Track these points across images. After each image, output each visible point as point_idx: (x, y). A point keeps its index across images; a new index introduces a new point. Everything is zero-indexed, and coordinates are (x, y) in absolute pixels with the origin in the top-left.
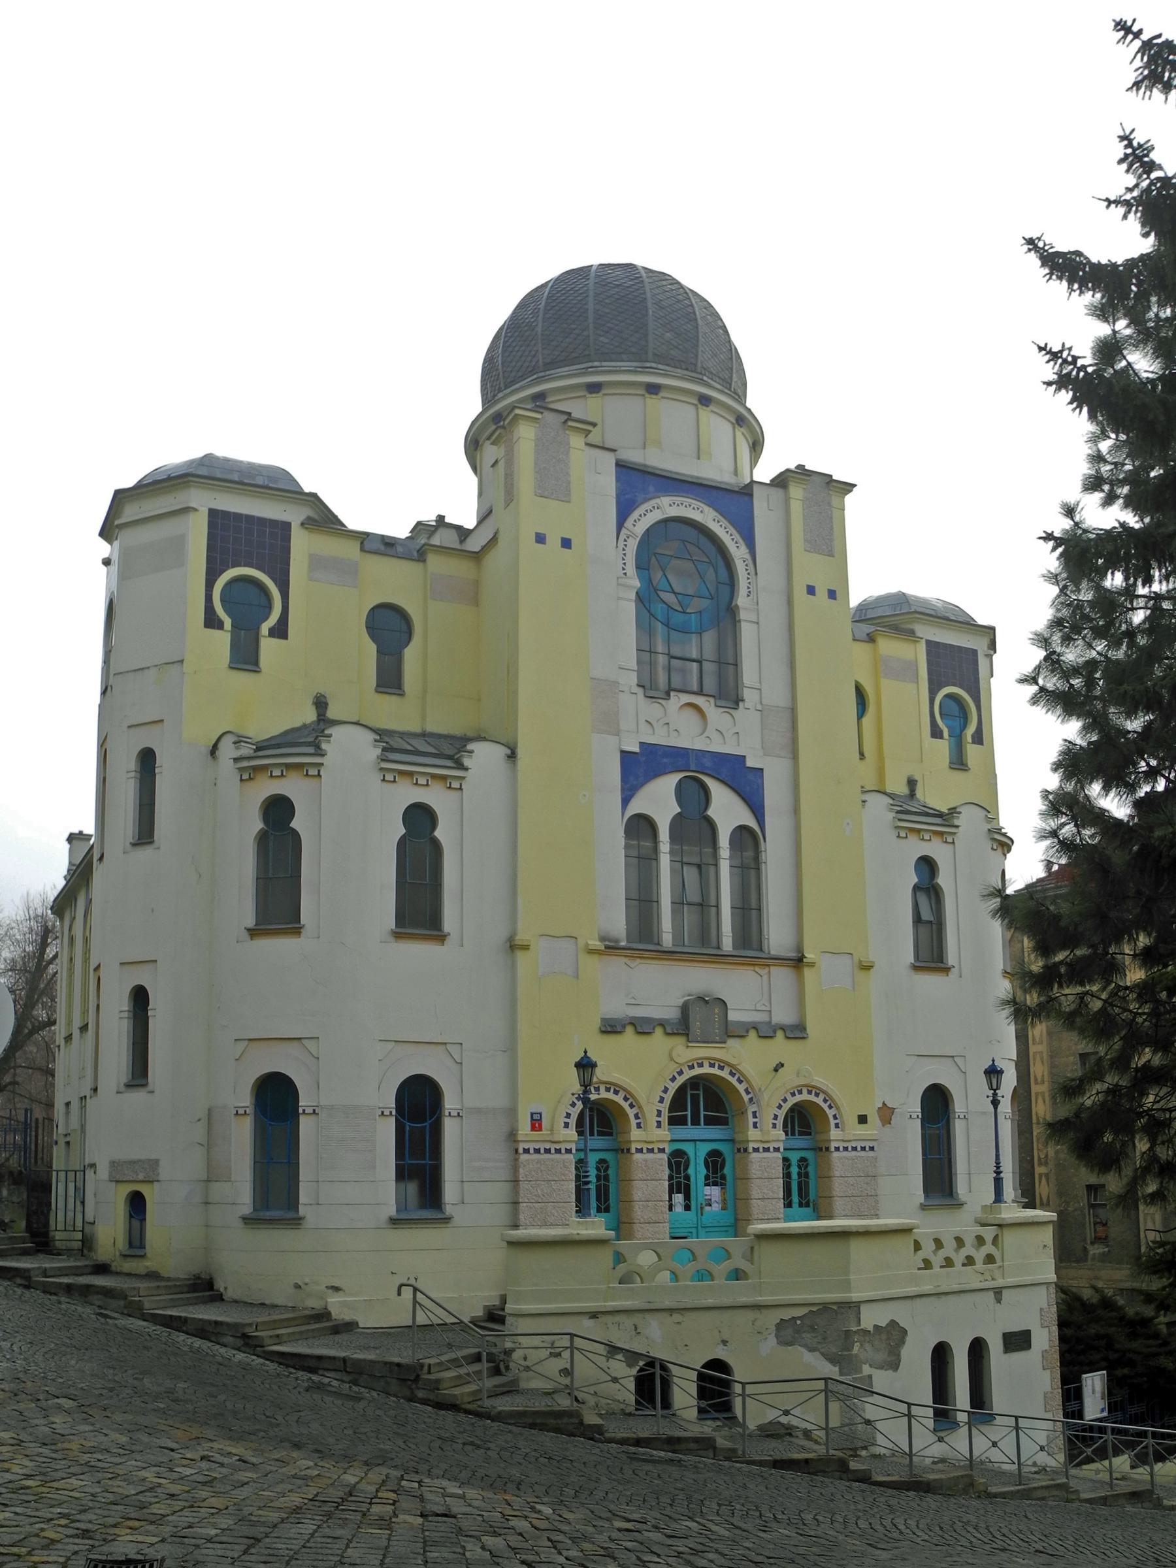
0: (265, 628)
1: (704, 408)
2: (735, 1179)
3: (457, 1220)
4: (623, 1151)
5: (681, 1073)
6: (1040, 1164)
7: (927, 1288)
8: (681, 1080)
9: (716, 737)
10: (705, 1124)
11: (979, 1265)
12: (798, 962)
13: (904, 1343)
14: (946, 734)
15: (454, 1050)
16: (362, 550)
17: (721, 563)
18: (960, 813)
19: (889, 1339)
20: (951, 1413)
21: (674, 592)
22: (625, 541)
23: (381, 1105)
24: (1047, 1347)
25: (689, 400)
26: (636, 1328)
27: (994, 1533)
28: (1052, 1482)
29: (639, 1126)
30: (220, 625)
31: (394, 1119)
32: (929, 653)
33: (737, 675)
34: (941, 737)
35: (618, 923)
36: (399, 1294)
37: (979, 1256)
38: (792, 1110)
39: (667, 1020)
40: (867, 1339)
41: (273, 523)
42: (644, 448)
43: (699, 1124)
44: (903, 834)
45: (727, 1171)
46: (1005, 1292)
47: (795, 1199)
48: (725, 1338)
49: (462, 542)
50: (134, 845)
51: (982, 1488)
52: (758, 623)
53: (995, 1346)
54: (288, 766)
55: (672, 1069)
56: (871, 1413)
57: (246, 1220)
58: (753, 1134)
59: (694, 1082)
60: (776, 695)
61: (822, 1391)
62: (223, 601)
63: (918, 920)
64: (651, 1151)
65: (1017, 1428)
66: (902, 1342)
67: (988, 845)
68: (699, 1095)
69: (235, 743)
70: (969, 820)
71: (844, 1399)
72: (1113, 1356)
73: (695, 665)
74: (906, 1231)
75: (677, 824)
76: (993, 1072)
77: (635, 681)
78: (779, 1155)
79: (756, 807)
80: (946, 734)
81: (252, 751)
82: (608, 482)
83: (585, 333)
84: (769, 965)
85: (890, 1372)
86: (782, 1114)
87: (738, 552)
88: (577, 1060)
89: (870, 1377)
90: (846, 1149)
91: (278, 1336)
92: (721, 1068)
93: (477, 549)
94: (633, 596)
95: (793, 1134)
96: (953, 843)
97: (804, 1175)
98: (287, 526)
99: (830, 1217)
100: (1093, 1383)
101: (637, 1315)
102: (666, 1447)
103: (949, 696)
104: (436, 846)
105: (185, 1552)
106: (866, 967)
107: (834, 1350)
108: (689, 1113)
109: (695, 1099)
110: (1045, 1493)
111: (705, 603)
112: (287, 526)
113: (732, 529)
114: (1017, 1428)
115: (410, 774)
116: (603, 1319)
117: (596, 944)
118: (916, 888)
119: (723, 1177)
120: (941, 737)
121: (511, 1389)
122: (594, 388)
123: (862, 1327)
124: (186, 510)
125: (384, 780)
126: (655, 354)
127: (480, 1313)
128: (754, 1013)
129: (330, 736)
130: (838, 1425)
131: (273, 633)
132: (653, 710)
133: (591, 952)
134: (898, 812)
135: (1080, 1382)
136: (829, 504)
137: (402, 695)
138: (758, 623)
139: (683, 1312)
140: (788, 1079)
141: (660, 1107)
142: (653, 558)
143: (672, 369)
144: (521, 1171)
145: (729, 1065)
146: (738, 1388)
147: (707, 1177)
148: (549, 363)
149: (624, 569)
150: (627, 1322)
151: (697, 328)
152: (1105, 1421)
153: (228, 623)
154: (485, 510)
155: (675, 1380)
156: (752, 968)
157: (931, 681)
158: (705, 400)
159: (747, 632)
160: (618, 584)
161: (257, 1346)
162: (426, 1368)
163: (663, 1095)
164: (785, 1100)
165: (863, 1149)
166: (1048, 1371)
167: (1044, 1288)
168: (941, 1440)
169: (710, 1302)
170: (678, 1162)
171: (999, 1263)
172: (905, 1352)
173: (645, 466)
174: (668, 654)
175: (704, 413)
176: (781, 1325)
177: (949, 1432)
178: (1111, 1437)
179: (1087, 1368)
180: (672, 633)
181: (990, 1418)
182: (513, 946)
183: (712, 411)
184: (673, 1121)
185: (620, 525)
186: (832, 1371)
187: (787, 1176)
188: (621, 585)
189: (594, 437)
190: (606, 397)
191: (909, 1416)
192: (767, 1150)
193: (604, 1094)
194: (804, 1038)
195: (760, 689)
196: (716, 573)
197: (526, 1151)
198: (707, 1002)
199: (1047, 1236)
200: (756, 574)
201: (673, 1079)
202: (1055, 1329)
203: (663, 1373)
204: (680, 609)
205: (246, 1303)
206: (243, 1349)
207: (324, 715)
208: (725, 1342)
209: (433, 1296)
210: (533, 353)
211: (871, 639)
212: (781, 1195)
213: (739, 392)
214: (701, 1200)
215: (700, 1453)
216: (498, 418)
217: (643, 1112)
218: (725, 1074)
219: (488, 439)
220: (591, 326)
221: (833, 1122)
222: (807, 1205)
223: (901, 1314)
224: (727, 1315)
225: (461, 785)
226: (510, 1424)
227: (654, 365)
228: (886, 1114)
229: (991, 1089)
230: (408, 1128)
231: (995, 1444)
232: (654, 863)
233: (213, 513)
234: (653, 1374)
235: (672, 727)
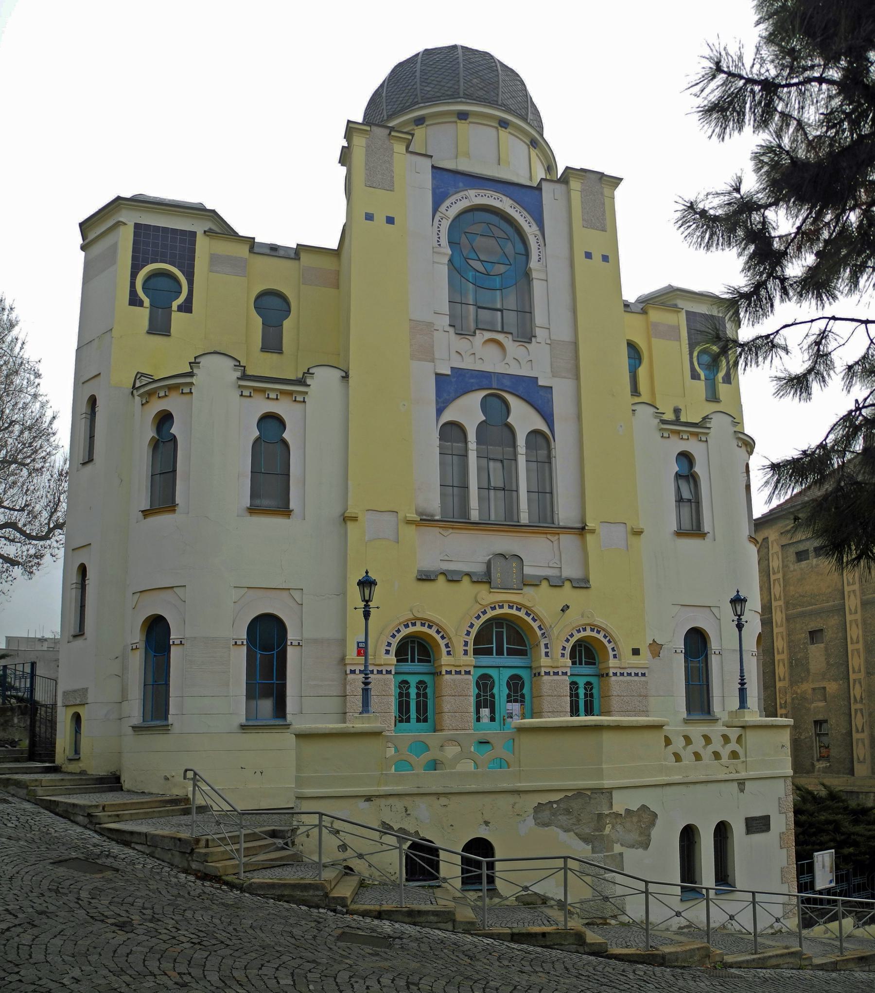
0: (175, 305)
2: (532, 697)
4: (603, 676)
9: (513, 363)
10: (508, 655)
11: (725, 760)
12: (582, 530)
13: (654, 825)
14: (703, 377)
15: (297, 595)
17: (517, 239)
18: (711, 419)
19: (639, 821)
21: (479, 260)
22: (440, 221)
23: (235, 637)
24: (784, 830)
26: (406, 810)
28: (786, 951)
29: (449, 653)
30: (141, 304)
31: (245, 648)
33: (532, 319)
35: (434, 504)
37: (725, 752)
40: (619, 820)
41: (183, 232)
43: (503, 655)
44: (666, 435)
45: (525, 691)
46: (747, 783)
48: (487, 819)
51: (718, 959)
53: (738, 829)
55: (477, 609)
57: (135, 728)
58: (544, 661)
59: (498, 621)
60: (563, 333)
61: (561, 869)
63: (680, 500)
65: (754, 903)
66: (653, 824)
67: (734, 443)
68: (503, 632)
70: (719, 424)
72: (839, 838)
73: (499, 313)
75: (481, 427)
76: (738, 601)
77: (448, 323)
78: (567, 680)
80: (703, 377)
82: (426, 179)
83: (415, 87)
84: (558, 534)
85: (640, 850)
86: (569, 646)
87: (530, 229)
89: (621, 854)
90: (622, 674)
91: (118, 816)
92: (519, 609)
96: (706, 441)
98: (193, 234)
100: (823, 859)
101: (407, 798)
102: (407, 920)
106: (638, 533)
107: (587, 831)
109: (500, 636)
110: (780, 961)
112: (193, 234)
113: (525, 212)
114: (754, 903)
115: (263, 391)
116: (377, 801)
117: (413, 516)
118: (678, 476)
119: (523, 696)
120: (699, 379)
121: (296, 860)
123: (614, 810)
124: (119, 224)
125: (242, 395)
126: (465, 94)
128: (548, 569)
131: (180, 309)
132: (462, 344)
133: (409, 522)
135: (812, 858)
136: (602, 194)
138: (547, 281)
139: (450, 796)
140: (573, 617)
142: (463, 236)
145: (525, 607)
147: (509, 696)
148: (391, 115)
149: (438, 241)
150: (399, 804)
151: (498, 76)
152: (835, 894)
153: (147, 302)
156: (545, 536)
158: (504, 124)
159: (538, 287)
160: (433, 252)
161: (97, 824)
163: (469, 629)
165: (636, 675)
166: (785, 850)
167: (782, 781)
169: (473, 787)
170: (485, 683)
171: (742, 759)
172: (655, 833)
175: (503, 133)
176: (539, 808)
177: (696, 902)
178: (841, 908)
179: (818, 847)
182: (346, 519)
184: (477, 652)
185: (435, 210)
186: (583, 850)
188: (436, 253)
190: (428, 127)
192: (556, 674)
194: (587, 588)
195: (549, 329)
199: (785, 737)
202: (791, 815)
205: (134, 792)
206: (88, 826)
208: (487, 823)
214: (503, 713)
215: (439, 925)
217: (452, 642)
218: (522, 614)
221: (611, 653)
223: (650, 799)
224: (488, 799)
225: (304, 398)
226: (259, 895)
227: (463, 100)
228: (656, 648)
229: (736, 615)
230: (259, 656)
233: (137, 226)
235: (477, 356)
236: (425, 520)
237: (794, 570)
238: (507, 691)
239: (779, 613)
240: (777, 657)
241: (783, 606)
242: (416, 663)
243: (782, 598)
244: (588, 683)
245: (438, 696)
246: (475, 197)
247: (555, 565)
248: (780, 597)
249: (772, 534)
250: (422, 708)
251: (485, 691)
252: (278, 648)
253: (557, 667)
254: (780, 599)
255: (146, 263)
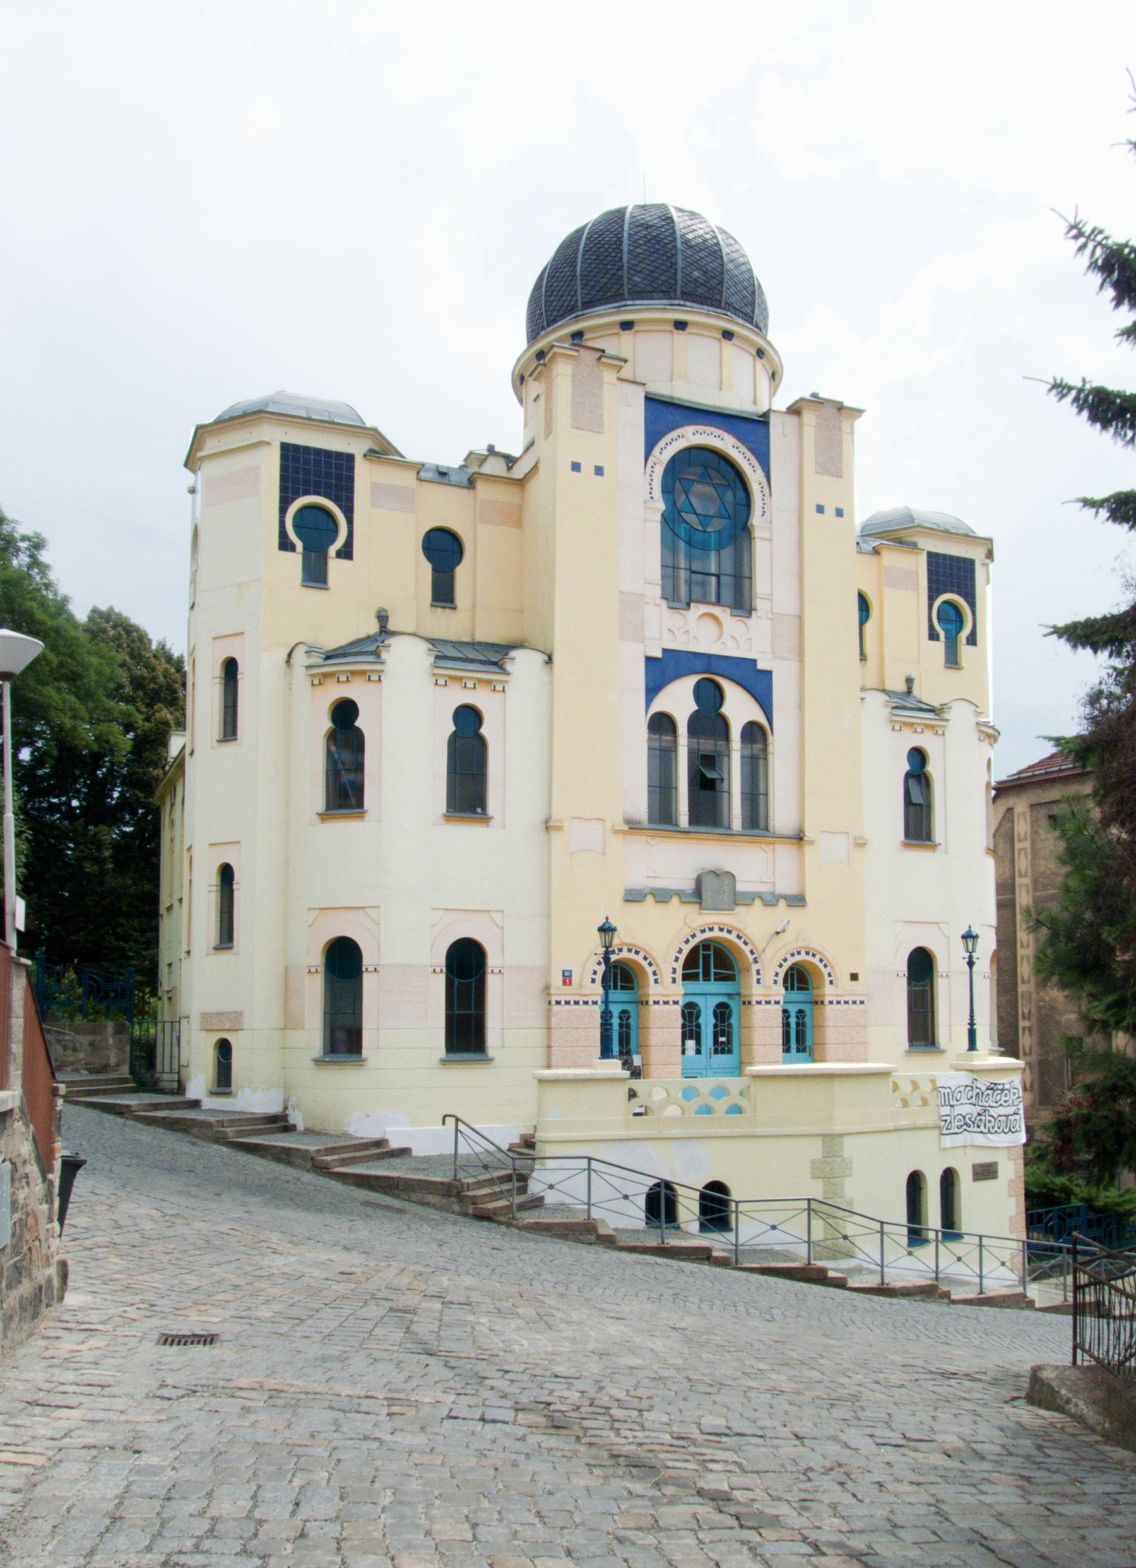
0: (332, 550)
1: (728, 341)
3: (497, 1061)
4: (818, 1003)
5: (694, 936)
6: (1024, 1018)
7: (905, 1123)
8: (693, 943)
12: (799, 838)
15: (497, 917)
16: (419, 479)
20: (924, 1232)
21: (695, 513)
25: (608, 332)
27: (940, 1330)
30: (293, 548)
32: (929, 564)
34: (938, 639)
35: (640, 806)
36: (444, 1124)
38: (791, 968)
39: (683, 891)
41: (339, 455)
42: (672, 381)
47: (793, 1045)
49: (509, 469)
50: (220, 741)
52: (771, 540)
54: (353, 673)
56: (850, 1230)
59: (706, 945)
60: (785, 603)
62: (295, 526)
64: (666, 1003)
65: (981, 1246)
67: (976, 735)
68: (709, 955)
69: (307, 652)
71: (825, 1217)
74: (884, 1074)
76: (969, 937)
78: (779, 1008)
79: (765, 703)
81: (322, 660)
83: (620, 273)
88: (600, 925)
90: (839, 1002)
93: (520, 476)
94: (659, 518)
95: (792, 989)
97: (801, 1025)
98: (350, 458)
99: (823, 1060)
103: (945, 602)
104: (482, 742)
105: (242, 1329)
106: (860, 844)
108: (701, 970)
109: (706, 958)
111: (725, 523)
112: (350, 458)
114: (981, 1246)
118: (908, 776)
120: (938, 639)
122: (627, 326)
126: (683, 292)
127: (517, 1141)
129: (389, 646)
130: (822, 1238)
134: (893, 708)
136: (840, 429)
137: (455, 608)
138: (771, 540)
140: (790, 941)
141: (676, 965)
143: (699, 306)
144: (553, 1019)
146: (733, 1206)
154: (529, 440)
155: (680, 1199)
157: (930, 589)
160: (645, 507)
162: (466, 1186)
163: (678, 955)
164: (785, 960)
168: (910, 1254)
170: (690, 1013)
173: (672, 398)
174: (690, 569)
180: (693, 549)
181: (958, 1236)
182: (549, 826)
183: (734, 345)
187: (786, 1025)
189: (626, 372)
191: (882, 1233)
192: (768, 1003)
193: (624, 955)
195: (771, 600)
196: (734, 495)
197: (558, 1003)
198: (717, 875)
200: (771, 495)
201: (687, 942)
203: (668, 1192)
204: (701, 529)
207: (385, 627)
209: (474, 1127)
210: (572, 293)
211: (876, 552)
212: (780, 1041)
213: (762, 326)
216: (541, 355)
219: (530, 375)
220: (625, 267)
221: (827, 979)
222: (804, 1050)
231: (959, 1259)
232: (673, 753)
233: (285, 447)
234: (659, 1193)
236: (633, 826)
237: (1046, 839)
238: (713, 1021)
239: (1024, 893)
240: (1020, 952)
241: (1030, 885)
242: (619, 991)
243: (1029, 875)
244: (800, 1011)
245: (643, 1028)
246: (691, 436)
247: (769, 880)
248: (1026, 872)
249: (1021, 804)
250: (625, 1040)
251: (691, 1021)
252: (476, 974)
253: (770, 995)
254: (1026, 876)
255: (297, 494)
